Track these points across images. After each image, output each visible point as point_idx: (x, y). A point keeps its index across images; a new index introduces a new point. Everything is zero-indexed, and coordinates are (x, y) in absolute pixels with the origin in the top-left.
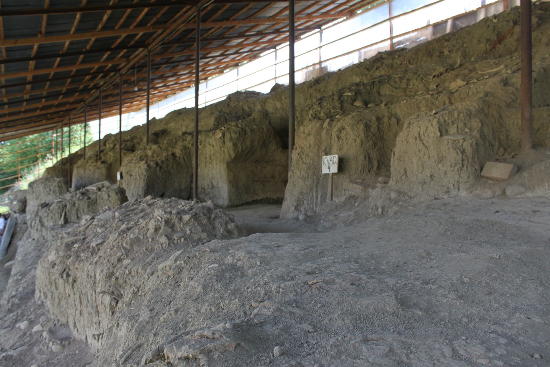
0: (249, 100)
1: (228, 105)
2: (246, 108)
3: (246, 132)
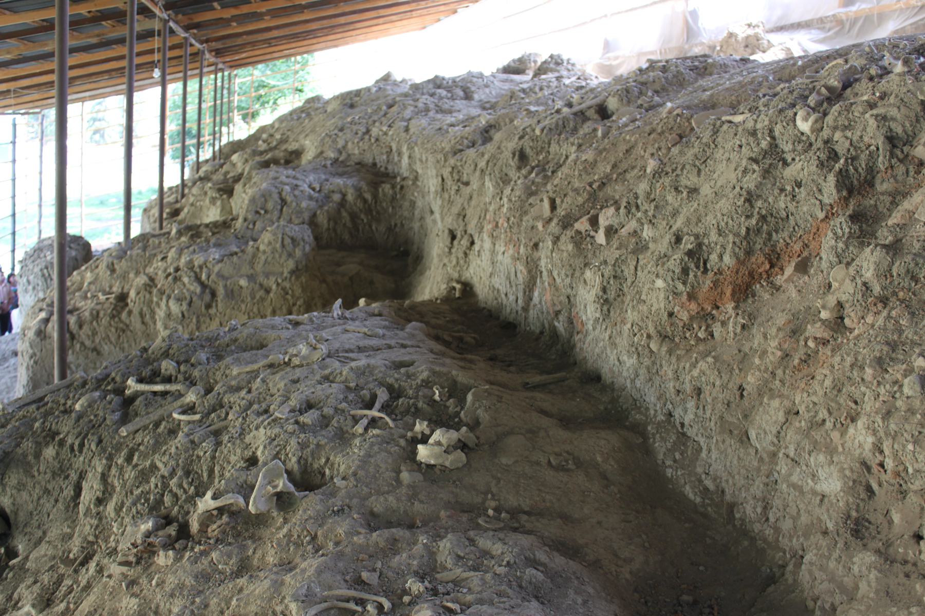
3: (213, 294)
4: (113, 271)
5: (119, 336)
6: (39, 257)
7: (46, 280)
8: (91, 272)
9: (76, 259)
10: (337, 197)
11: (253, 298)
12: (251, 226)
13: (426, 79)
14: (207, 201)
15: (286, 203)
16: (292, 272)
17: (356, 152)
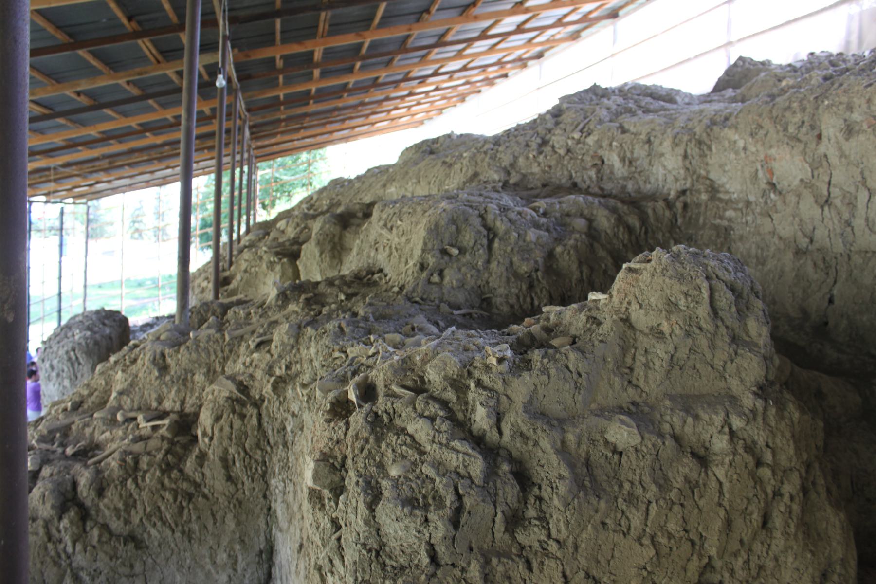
0: (629, 122)
1: (544, 143)
2: (614, 159)
3: (523, 478)
4: (164, 369)
5: (181, 508)
6: (66, 337)
7: (73, 365)
8: (123, 371)
9: (111, 338)
10: (580, 223)
11: (664, 485)
12: (436, 278)
13: (582, 89)
14: (264, 266)
15: (495, 235)
16: (762, 391)
17: (536, 169)
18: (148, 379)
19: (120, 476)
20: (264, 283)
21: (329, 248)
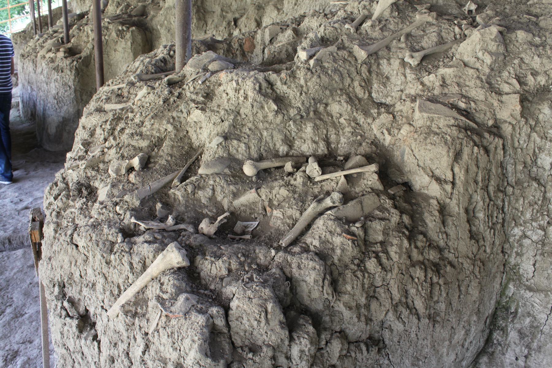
18: (260, 116)
19: (354, 258)
20: (115, 50)
21: (195, 10)
